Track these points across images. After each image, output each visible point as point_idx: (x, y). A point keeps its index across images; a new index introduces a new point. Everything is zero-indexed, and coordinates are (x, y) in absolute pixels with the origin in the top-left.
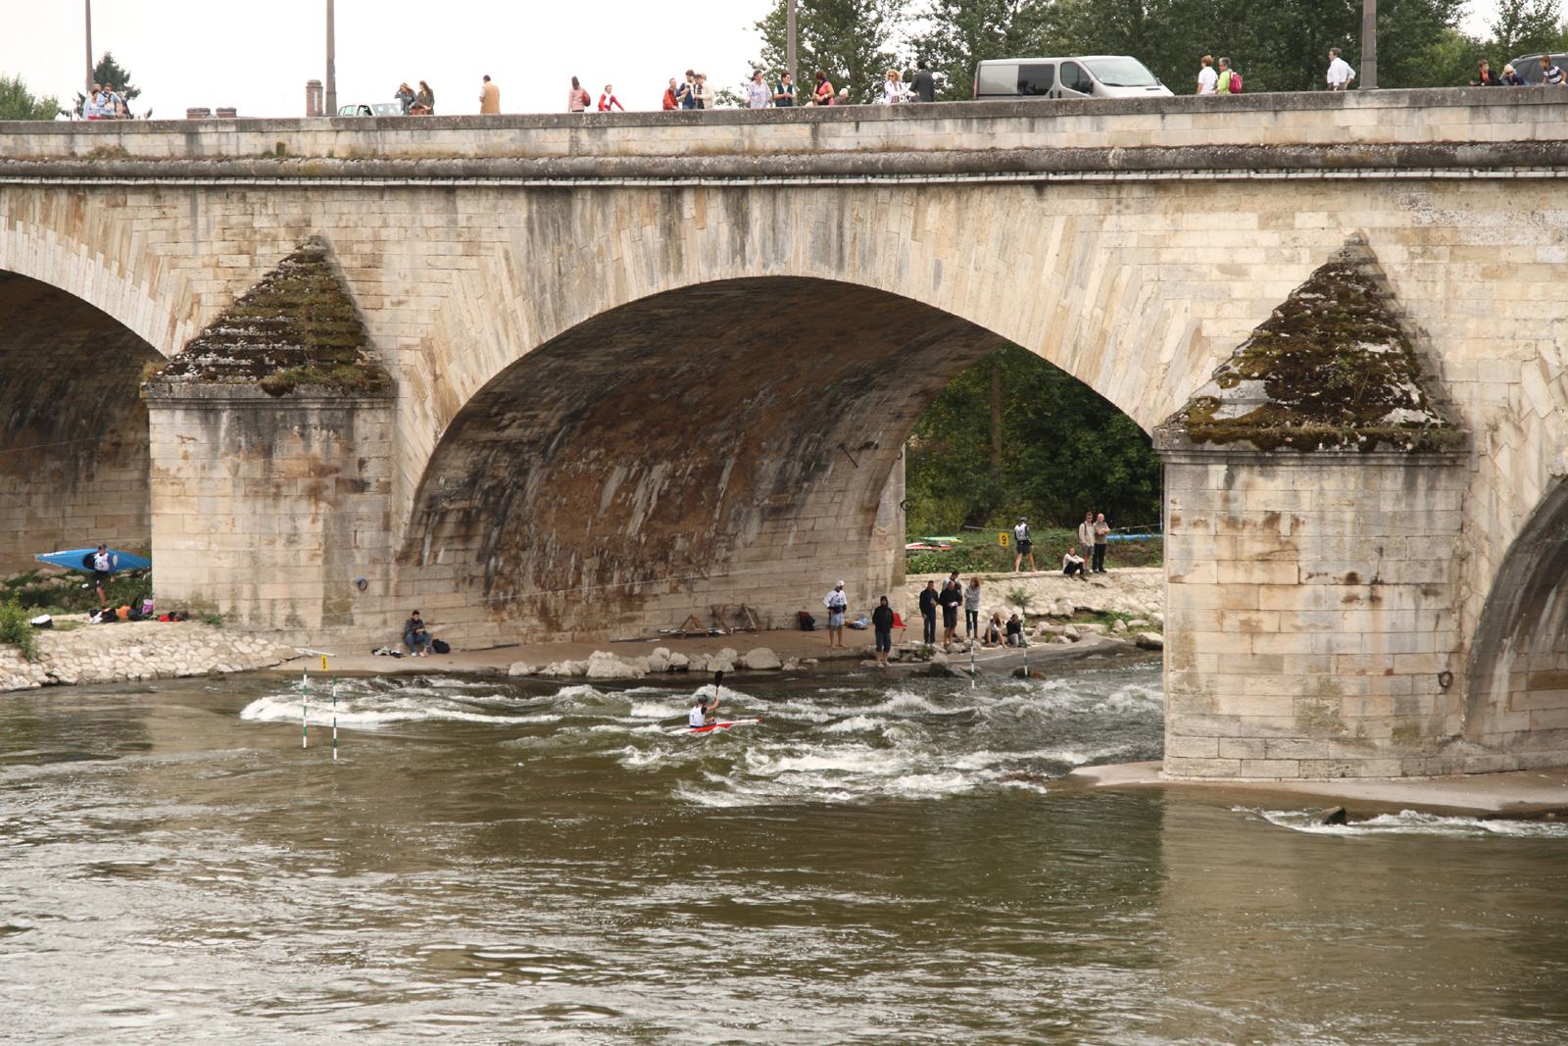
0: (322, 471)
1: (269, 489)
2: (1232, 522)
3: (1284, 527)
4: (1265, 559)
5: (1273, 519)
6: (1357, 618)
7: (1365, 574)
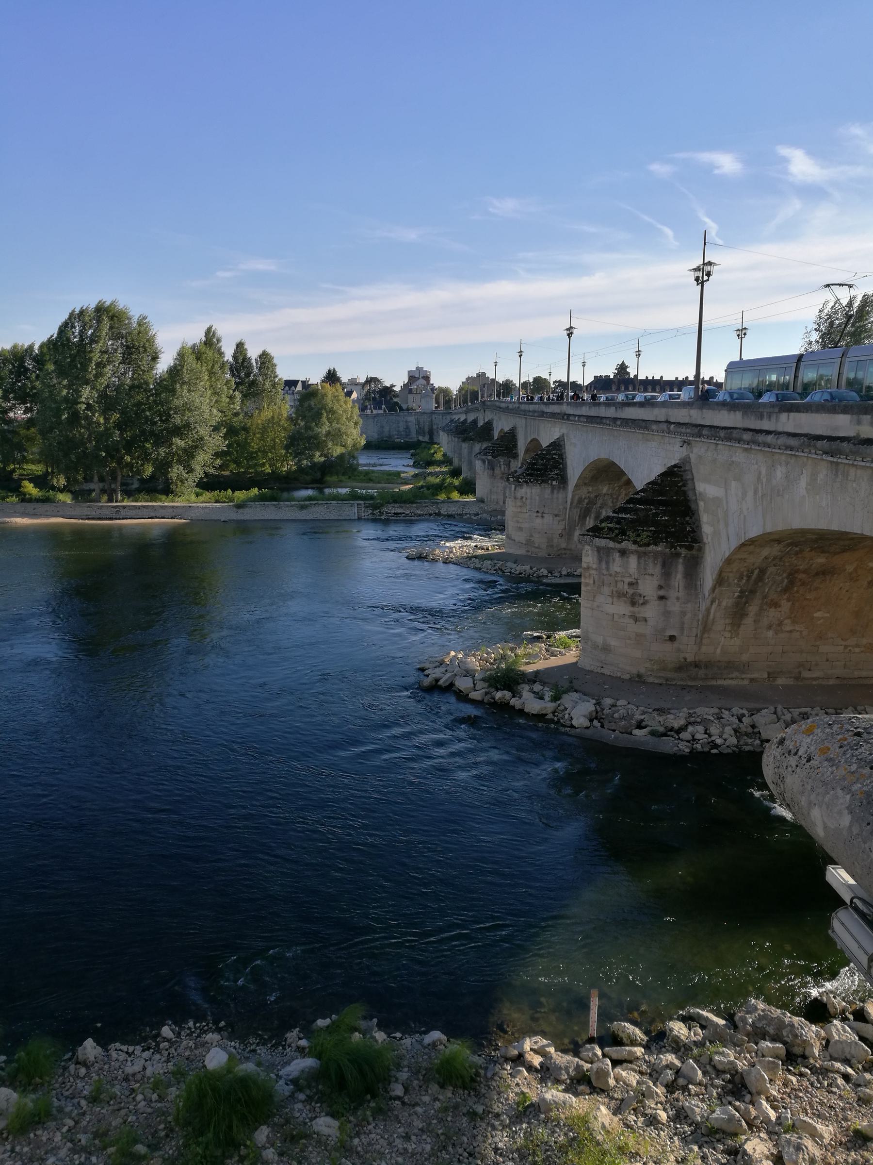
0: (503, 474)
1: (493, 476)
2: (515, 498)
4: (521, 507)
5: (522, 498)
6: (539, 521)
7: (541, 511)
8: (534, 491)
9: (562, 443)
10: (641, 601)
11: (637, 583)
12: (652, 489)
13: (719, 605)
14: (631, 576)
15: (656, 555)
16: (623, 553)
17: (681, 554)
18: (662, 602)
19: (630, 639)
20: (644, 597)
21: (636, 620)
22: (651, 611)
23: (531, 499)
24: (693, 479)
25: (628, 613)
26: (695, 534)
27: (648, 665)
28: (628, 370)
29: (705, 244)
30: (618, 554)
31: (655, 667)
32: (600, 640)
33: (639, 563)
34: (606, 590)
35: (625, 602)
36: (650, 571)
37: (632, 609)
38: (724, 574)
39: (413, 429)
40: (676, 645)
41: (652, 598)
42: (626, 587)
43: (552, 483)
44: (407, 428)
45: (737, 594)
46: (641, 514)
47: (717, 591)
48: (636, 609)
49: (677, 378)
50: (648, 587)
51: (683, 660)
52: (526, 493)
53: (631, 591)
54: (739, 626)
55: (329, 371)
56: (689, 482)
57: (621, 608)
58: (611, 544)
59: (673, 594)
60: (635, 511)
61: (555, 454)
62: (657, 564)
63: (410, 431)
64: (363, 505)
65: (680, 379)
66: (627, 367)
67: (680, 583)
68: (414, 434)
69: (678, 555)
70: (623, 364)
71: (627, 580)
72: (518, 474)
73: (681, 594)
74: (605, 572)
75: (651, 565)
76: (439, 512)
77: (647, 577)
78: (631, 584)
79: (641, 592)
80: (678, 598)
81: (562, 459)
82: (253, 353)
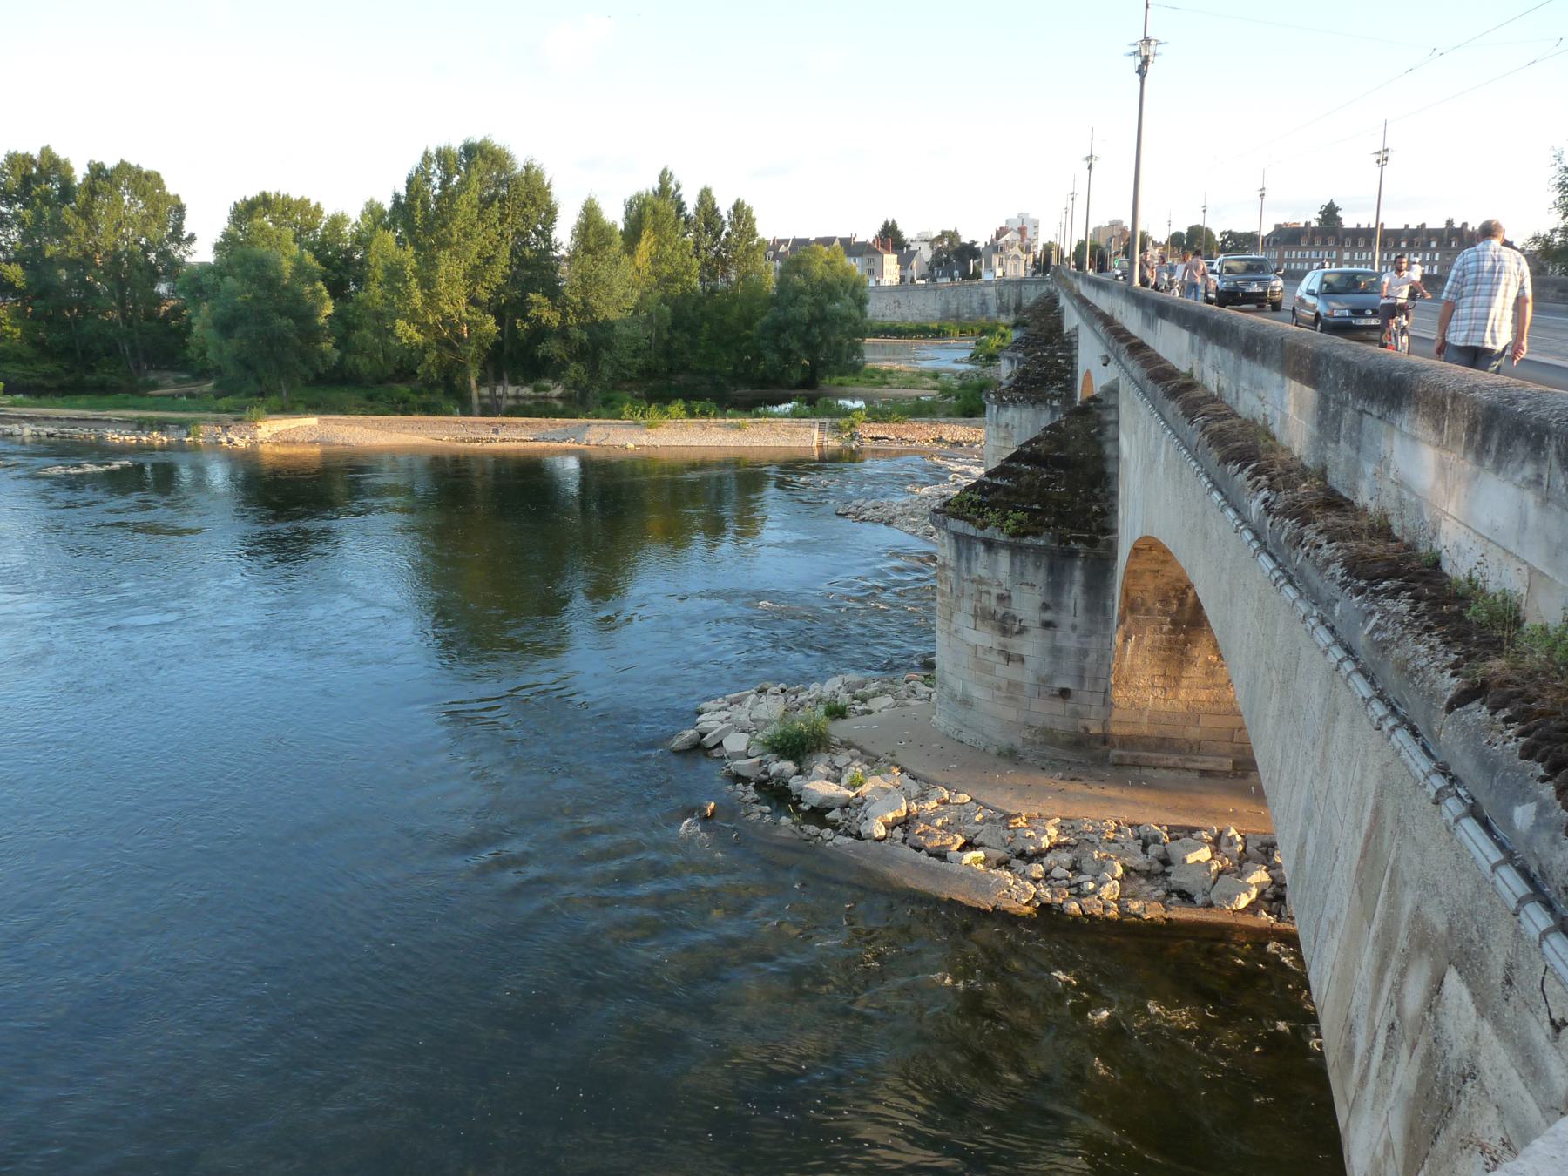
2: (998, 425)
3: (1010, 427)
5: (1007, 425)
8: (1024, 415)
9: (1074, 339)
10: (1016, 628)
11: (1010, 597)
12: (1049, 437)
13: (1138, 644)
14: (1000, 585)
15: (1039, 551)
16: (990, 545)
17: (1079, 553)
18: (1048, 632)
19: (999, 688)
20: (1020, 621)
21: (1009, 658)
22: (1031, 646)
23: (1020, 427)
24: (1117, 423)
25: (996, 647)
26: (1105, 519)
27: (1026, 734)
28: (1339, 214)
29: (1147, 6)
30: (982, 547)
31: (1037, 739)
32: (958, 687)
33: (1012, 564)
34: (967, 605)
35: (993, 627)
36: (1029, 578)
37: (1002, 639)
38: (1133, 594)
39: (993, 305)
40: (1070, 705)
41: (1032, 624)
42: (994, 602)
43: (1051, 402)
44: (984, 303)
45: (1166, 628)
46: (1025, 479)
47: (1129, 619)
48: (1007, 640)
49: (1407, 226)
50: (1027, 605)
51: (1082, 731)
52: (1013, 417)
53: (1001, 611)
54: (1177, 680)
55: (887, 223)
56: (1111, 428)
57: (985, 637)
58: (971, 531)
59: (1066, 619)
60: (1019, 474)
61: (1061, 357)
62: (1039, 567)
63: (987, 309)
64: (828, 425)
65: (1413, 226)
66: (1337, 209)
67: (1078, 602)
68: (993, 311)
69: (1073, 554)
70: (1331, 205)
71: (995, 591)
72: (1003, 387)
73: (1080, 619)
74: (965, 575)
75: (1031, 569)
76: (941, 437)
77: (1024, 587)
78: (1001, 598)
79: (1016, 613)
80: (1074, 627)
81: (1072, 364)
82: (724, 207)
